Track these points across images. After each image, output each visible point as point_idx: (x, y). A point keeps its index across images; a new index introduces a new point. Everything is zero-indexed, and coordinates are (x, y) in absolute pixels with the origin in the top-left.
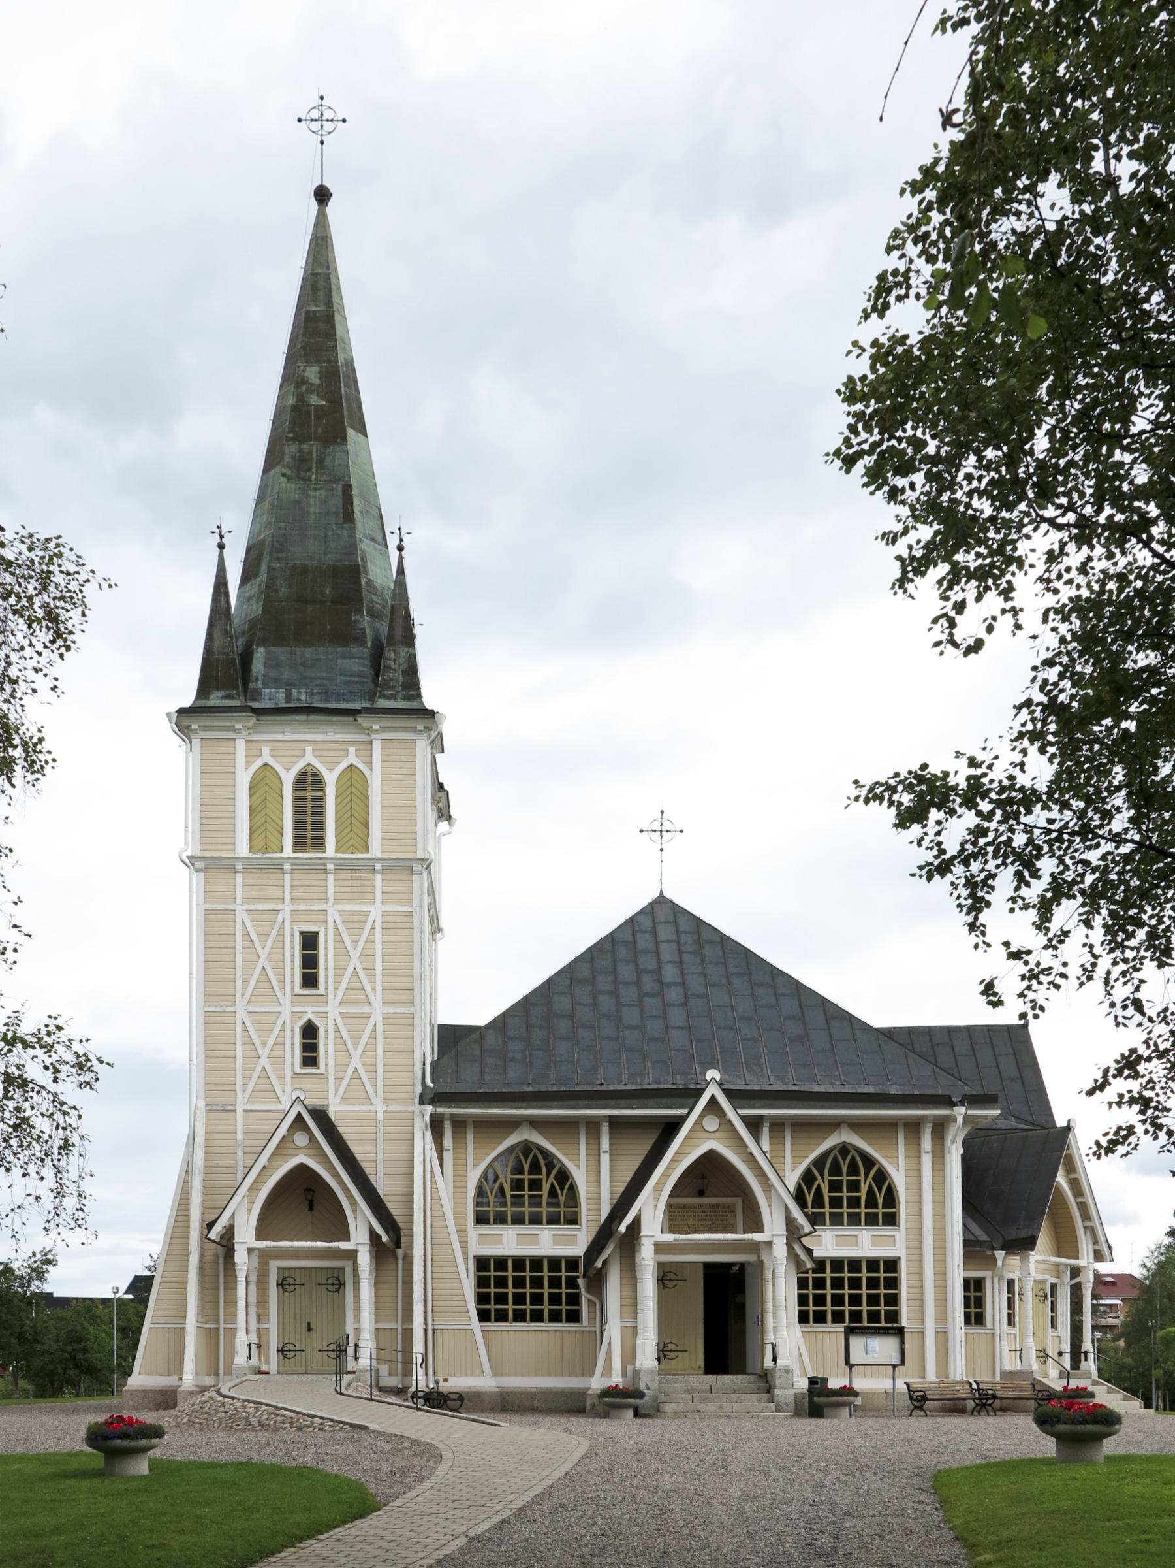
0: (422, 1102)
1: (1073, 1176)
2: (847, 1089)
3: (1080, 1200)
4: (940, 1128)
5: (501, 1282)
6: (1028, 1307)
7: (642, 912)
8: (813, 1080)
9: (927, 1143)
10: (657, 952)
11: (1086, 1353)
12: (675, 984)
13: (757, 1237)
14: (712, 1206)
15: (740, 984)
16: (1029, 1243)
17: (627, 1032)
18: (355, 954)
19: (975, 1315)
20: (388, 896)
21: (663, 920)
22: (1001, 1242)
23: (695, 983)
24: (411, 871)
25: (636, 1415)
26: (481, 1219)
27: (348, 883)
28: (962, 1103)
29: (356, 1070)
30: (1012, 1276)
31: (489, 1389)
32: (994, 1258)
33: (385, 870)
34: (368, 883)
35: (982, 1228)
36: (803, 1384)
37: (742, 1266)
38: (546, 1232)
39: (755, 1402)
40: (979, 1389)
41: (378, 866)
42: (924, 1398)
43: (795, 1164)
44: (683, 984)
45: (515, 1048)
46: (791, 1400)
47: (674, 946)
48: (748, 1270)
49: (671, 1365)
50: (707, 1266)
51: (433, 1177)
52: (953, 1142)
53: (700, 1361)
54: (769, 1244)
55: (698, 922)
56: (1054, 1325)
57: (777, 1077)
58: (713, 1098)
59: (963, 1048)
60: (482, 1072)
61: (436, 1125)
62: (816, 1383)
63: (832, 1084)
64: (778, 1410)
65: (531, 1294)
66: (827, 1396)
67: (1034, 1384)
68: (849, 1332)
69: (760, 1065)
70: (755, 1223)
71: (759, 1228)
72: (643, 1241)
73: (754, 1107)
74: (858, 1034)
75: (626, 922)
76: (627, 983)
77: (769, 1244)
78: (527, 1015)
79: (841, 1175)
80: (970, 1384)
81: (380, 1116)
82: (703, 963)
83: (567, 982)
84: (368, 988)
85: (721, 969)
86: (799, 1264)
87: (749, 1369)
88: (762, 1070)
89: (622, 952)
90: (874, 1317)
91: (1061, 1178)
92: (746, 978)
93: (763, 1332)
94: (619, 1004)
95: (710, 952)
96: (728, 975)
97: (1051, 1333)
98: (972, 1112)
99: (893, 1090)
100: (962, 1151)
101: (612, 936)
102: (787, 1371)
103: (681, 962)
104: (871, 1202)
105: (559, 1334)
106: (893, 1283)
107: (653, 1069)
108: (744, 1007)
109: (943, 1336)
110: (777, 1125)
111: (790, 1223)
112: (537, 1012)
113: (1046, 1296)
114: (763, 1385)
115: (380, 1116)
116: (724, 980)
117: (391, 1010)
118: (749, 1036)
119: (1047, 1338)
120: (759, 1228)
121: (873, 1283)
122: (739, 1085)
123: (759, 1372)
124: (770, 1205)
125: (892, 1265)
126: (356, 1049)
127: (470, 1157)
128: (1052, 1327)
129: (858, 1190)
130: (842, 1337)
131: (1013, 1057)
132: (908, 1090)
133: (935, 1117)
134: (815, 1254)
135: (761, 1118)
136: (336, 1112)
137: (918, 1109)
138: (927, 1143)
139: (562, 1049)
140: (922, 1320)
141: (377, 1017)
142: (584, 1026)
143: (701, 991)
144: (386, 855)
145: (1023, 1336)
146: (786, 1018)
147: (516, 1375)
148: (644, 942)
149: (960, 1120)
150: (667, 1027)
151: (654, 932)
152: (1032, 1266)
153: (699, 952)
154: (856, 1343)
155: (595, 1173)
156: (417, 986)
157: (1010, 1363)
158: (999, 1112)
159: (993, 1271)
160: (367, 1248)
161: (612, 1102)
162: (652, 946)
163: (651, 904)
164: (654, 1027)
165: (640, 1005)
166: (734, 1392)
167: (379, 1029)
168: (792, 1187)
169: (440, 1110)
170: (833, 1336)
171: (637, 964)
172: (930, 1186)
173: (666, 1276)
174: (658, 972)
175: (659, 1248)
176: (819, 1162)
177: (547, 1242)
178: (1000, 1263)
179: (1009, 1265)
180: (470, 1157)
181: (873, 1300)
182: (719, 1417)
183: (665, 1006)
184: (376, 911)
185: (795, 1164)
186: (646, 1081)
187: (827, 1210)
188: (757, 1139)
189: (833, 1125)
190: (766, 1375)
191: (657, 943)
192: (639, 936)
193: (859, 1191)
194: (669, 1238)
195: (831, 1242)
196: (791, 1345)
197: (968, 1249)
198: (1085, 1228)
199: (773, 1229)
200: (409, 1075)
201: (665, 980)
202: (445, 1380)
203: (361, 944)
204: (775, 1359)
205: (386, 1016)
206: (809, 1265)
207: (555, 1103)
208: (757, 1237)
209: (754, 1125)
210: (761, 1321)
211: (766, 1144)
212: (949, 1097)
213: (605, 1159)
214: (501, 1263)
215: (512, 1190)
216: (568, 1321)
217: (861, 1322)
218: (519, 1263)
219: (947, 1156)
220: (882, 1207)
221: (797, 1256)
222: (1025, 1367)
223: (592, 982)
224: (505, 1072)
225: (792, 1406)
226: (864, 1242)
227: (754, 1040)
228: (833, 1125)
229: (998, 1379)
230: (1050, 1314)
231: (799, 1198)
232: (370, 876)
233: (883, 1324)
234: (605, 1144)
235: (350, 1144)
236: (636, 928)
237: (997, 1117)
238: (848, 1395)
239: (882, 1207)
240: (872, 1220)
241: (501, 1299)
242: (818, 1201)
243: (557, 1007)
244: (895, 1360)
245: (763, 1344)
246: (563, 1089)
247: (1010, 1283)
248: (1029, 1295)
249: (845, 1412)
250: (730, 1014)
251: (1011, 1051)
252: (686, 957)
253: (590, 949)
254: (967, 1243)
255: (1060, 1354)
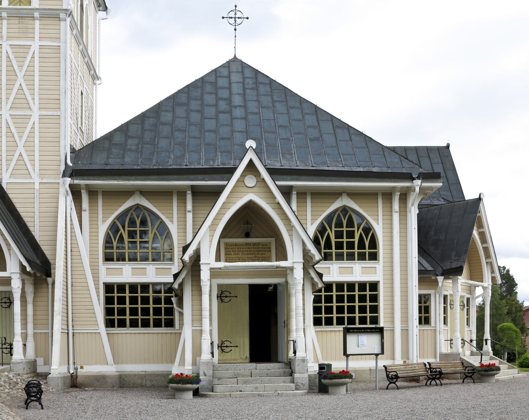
0: (64, 176)
1: (481, 230)
2: (346, 169)
3: (485, 245)
4: (404, 196)
5: (122, 300)
6: (457, 313)
7: (222, 66)
8: (325, 163)
9: (396, 206)
10: (230, 89)
11: (486, 340)
12: (240, 106)
13: (282, 264)
14: (254, 244)
15: (280, 107)
16: (458, 271)
17: (207, 134)
18: (20, 75)
19: (425, 319)
20: (43, 35)
21: (235, 70)
22: (440, 271)
23: (253, 106)
24: (59, 18)
25: (194, 395)
26: (108, 258)
27: (17, 26)
28: (418, 178)
29: (20, 155)
30: (446, 293)
31: (110, 374)
32: (436, 282)
33: (41, 17)
34: (30, 26)
35: (428, 262)
36: (314, 368)
37: (275, 286)
38: (151, 266)
39: (282, 384)
40: (430, 368)
41: (36, 15)
42: (397, 377)
43: (313, 220)
44: (245, 106)
45: (132, 143)
46: (306, 381)
47: (241, 85)
48: (279, 289)
49: (227, 356)
50: (252, 287)
51: (72, 228)
52: (413, 205)
53: (247, 354)
54: (292, 269)
55: (257, 72)
56: (468, 324)
57: (302, 161)
58: (251, 161)
59: (413, 157)
60: (108, 158)
61: (76, 193)
62: (324, 368)
63: (337, 166)
64: (297, 389)
65: (141, 308)
66: (331, 378)
67: (463, 362)
68: (347, 331)
69: (291, 154)
70: (282, 255)
71: (284, 257)
72: (202, 267)
73: (286, 180)
74: (353, 137)
75: (212, 71)
76: (209, 106)
77: (292, 269)
78: (143, 123)
79: (343, 227)
80: (425, 365)
81: (37, 186)
82: (258, 95)
83: (171, 104)
84: (29, 98)
85: (269, 98)
86: (314, 284)
87: (280, 359)
88: (292, 158)
89: (208, 88)
90: (363, 320)
91: (475, 233)
92: (284, 103)
93: (288, 332)
94: (203, 118)
95: (263, 89)
96: (273, 102)
97: (466, 328)
98: (425, 184)
99: (375, 170)
100: (417, 211)
101: (202, 78)
102: (304, 360)
103: (244, 94)
104: (362, 245)
105: (160, 335)
106: (375, 298)
107: (221, 156)
108: (283, 120)
109: (405, 331)
110: (302, 194)
111: (306, 254)
112: (150, 122)
113: (464, 306)
114: (288, 370)
115: (37, 186)
116: (270, 105)
117: (44, 113)
118: (285, 137)
119: (465, 332)
120: (284, 257)
121: (362, 299)
122: (277, 166)
123: (285, 361)
124: (292, 241)
125: (374, 286)
126: (20, 140)
127: (100, 216)
128: (444, 323)
129: (353, 237)
130: (342, 334)
131: (441, 165)
132: (385, 170)
133: (402, 187)
134: (325, 279)
135: (291, 187)
136: (7, 183)
137: (391, 182)
138: (396, 206)
139: (163, 143)
140: (393, 322)
141: (35, 118)
142: (179, 130)
143: (256, 110)
144: (42, 7)
145: (453, 331)
146: (308, 127)
147: (132, 363)
148: (222, 82)
149: (417, 189)
150: (233, 131)
151: (229, 77)
152: (460, 287)
153: (256, 89)
154: (352, 339)
155: (176, 220)
156: (62, 97)
157: (445, 348)
158: (441, 184)
159: (436, 289)
160: (18, 276)
161: (192, 177)
162: (227, 85)
163: (229, 62)
164: (225, 131)
165: (216, 118)
166: (267, 375)
167: (37, 126)
168: (311, 235)
169: (76, 182)
170: (337, 333)
171: (216, 94)
172: (398, 233)
173: (224, 295)
174: (229, 100)
175: (214, 273)
176: (329, 219)
177: (151, 274)
178: (440, 284)
179: (446, 286)
180: (100, 216)
181: (362, 310)
182: (254, 396)
183: (232, 119)
184: (35, 45)
185: (313, 220)
186: (216, 164)
187: (334, 251)
188: (289, 203)
189: (336, 194)
190: (290, 363)
191: (230, 83)
192: (219, 79)
193: (354, 238)
194: (222, 264)
195: (335, 272)
196: (308, 342)
197: (422, 276)
198: (487, 263)
199: (294, 258)
200: (56, 158)
201: (234, 104)
202: (82, 368)
203: (25, 68)
204: (295, 352)
205: (41, 117)
206: (320, 285)
207: (155, 177)
208: (282, 264)
209: (287, 192)
210: (287, 324)
211: (294, 207)
212: (411, 174)
213: (190, 216)
214: (121, 287)
215: (335, 238)
216: (166, 326)
217: (355, 324)
218: (133, 287)
219: (409, 215)
220: (366, 248)
221: (312, 279)
222: (454, 350)
223: (187, 105)
224: (124, 157)
225: (307, 386)
226: (356, 272)
227: (288, 139)
228: (336, 194)
229: (438, 360)
230: (466, 317)
231: (316, 242)
232: (31, 22)
233: (368, 326)
234: (189, 207)
235: (17, 205)
236: (218, 74)
237: (439, 189)
238: (346, 377)
239: (366, 248)
240: (362, 257)
241: (122, 312)
242: (328, 245)
243: (163, 119)
244: (377, 350)
245: (288, 341)
246: (161, 167)
247: (445, 297)
248: (457, 304)
249: (343, 389)
250: (273, 124)
251: (440, 162)
252: (248, 91)
253: (188, 86)
254: (420, 272)
255: (471, 341)
